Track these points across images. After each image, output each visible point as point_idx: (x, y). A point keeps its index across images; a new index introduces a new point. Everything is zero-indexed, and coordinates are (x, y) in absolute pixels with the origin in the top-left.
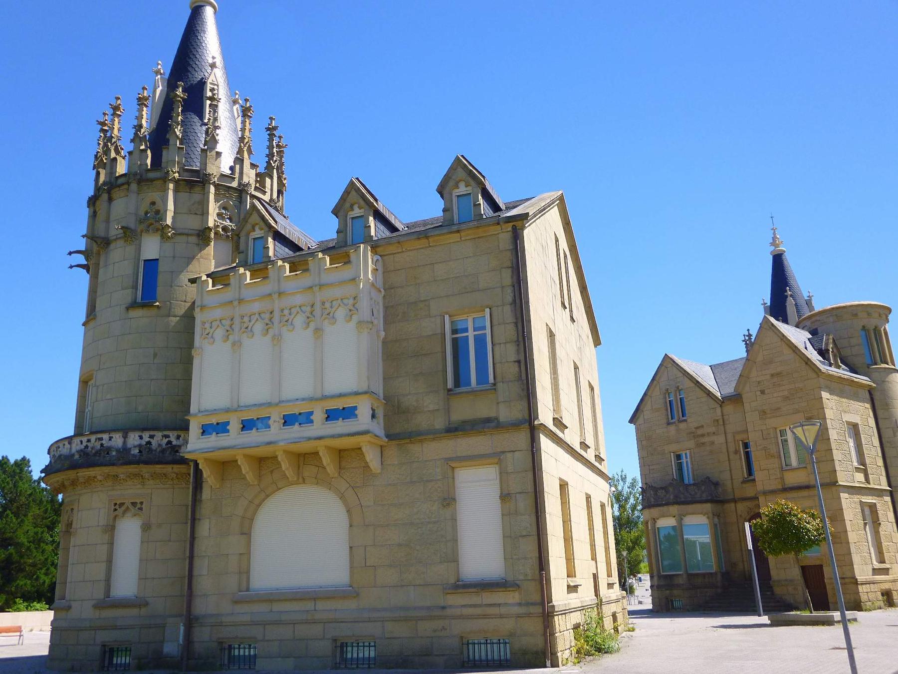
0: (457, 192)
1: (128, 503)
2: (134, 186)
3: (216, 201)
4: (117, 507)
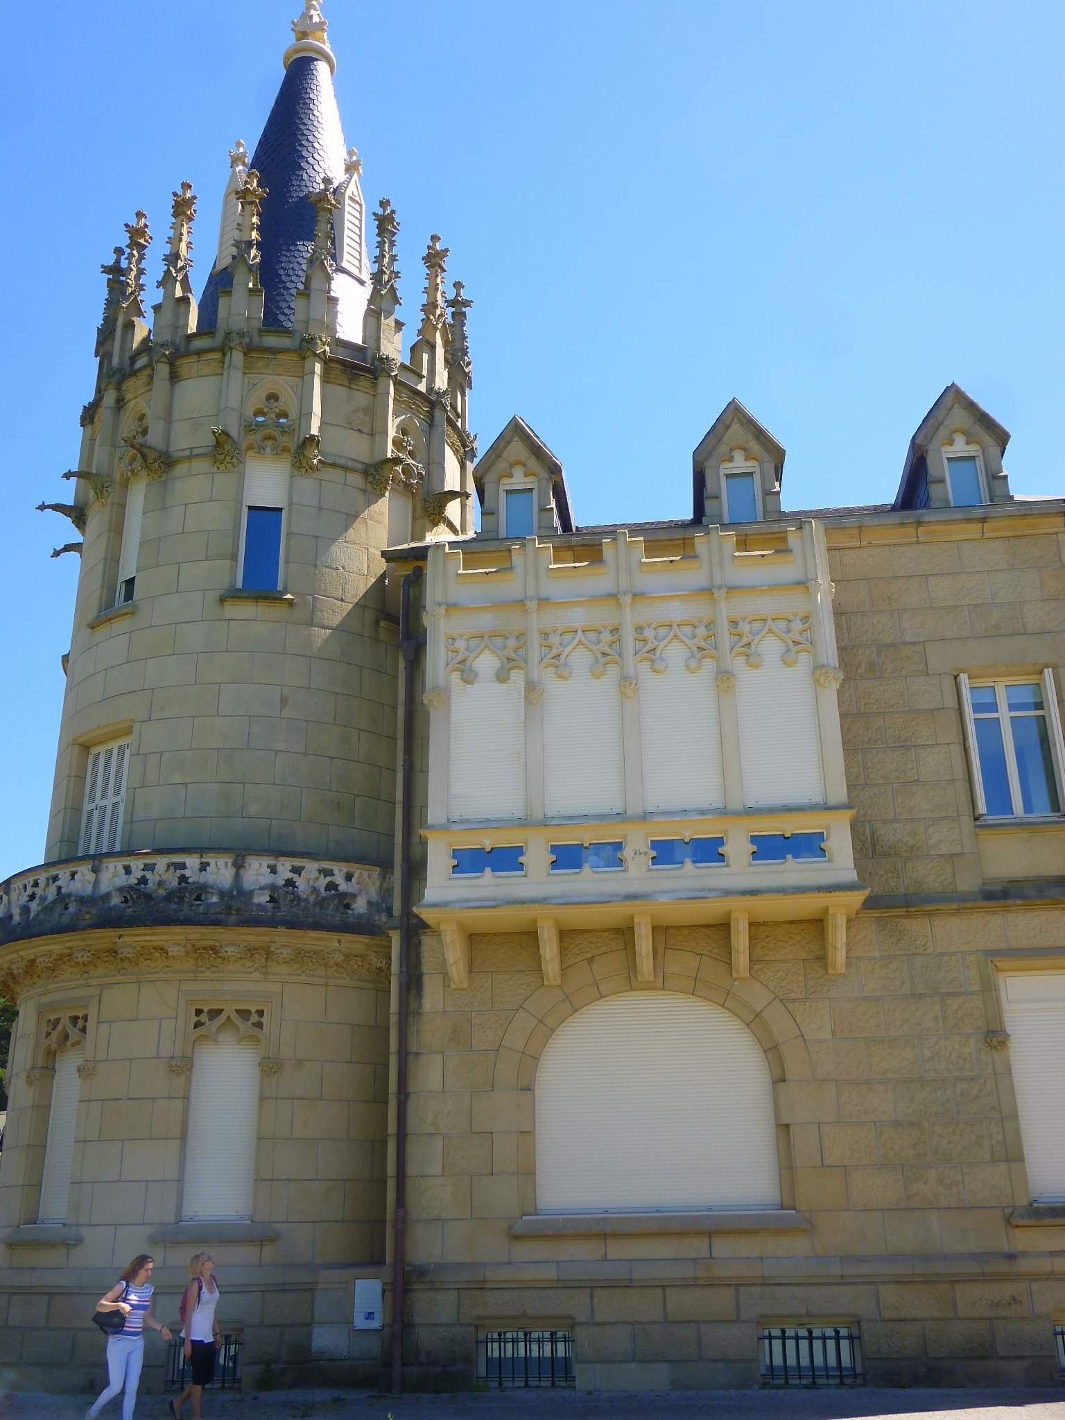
0: (508, 484)
1: (229, 1009)
2: (237, 357)
3: (396, 415)
4: (204, 1018)
